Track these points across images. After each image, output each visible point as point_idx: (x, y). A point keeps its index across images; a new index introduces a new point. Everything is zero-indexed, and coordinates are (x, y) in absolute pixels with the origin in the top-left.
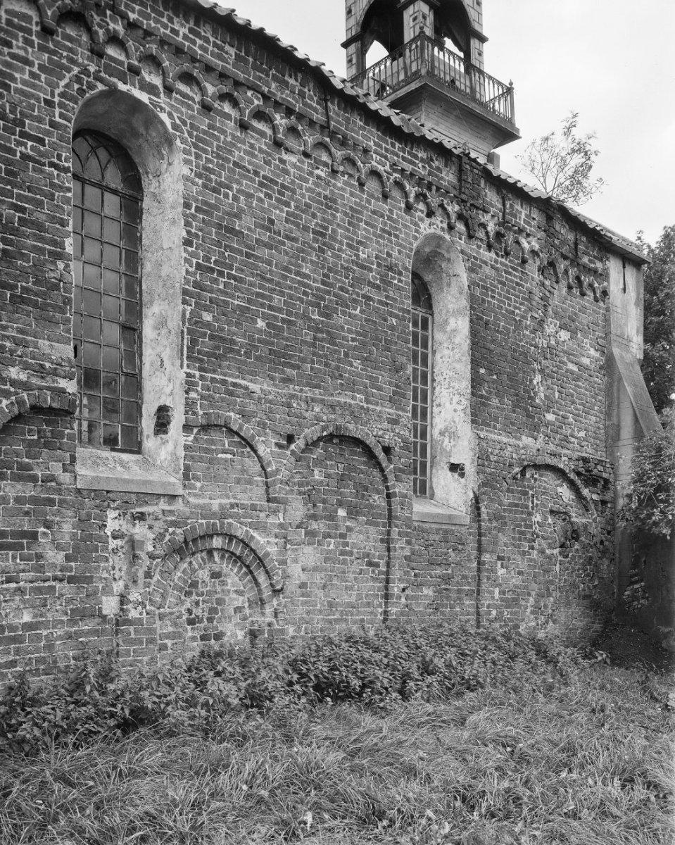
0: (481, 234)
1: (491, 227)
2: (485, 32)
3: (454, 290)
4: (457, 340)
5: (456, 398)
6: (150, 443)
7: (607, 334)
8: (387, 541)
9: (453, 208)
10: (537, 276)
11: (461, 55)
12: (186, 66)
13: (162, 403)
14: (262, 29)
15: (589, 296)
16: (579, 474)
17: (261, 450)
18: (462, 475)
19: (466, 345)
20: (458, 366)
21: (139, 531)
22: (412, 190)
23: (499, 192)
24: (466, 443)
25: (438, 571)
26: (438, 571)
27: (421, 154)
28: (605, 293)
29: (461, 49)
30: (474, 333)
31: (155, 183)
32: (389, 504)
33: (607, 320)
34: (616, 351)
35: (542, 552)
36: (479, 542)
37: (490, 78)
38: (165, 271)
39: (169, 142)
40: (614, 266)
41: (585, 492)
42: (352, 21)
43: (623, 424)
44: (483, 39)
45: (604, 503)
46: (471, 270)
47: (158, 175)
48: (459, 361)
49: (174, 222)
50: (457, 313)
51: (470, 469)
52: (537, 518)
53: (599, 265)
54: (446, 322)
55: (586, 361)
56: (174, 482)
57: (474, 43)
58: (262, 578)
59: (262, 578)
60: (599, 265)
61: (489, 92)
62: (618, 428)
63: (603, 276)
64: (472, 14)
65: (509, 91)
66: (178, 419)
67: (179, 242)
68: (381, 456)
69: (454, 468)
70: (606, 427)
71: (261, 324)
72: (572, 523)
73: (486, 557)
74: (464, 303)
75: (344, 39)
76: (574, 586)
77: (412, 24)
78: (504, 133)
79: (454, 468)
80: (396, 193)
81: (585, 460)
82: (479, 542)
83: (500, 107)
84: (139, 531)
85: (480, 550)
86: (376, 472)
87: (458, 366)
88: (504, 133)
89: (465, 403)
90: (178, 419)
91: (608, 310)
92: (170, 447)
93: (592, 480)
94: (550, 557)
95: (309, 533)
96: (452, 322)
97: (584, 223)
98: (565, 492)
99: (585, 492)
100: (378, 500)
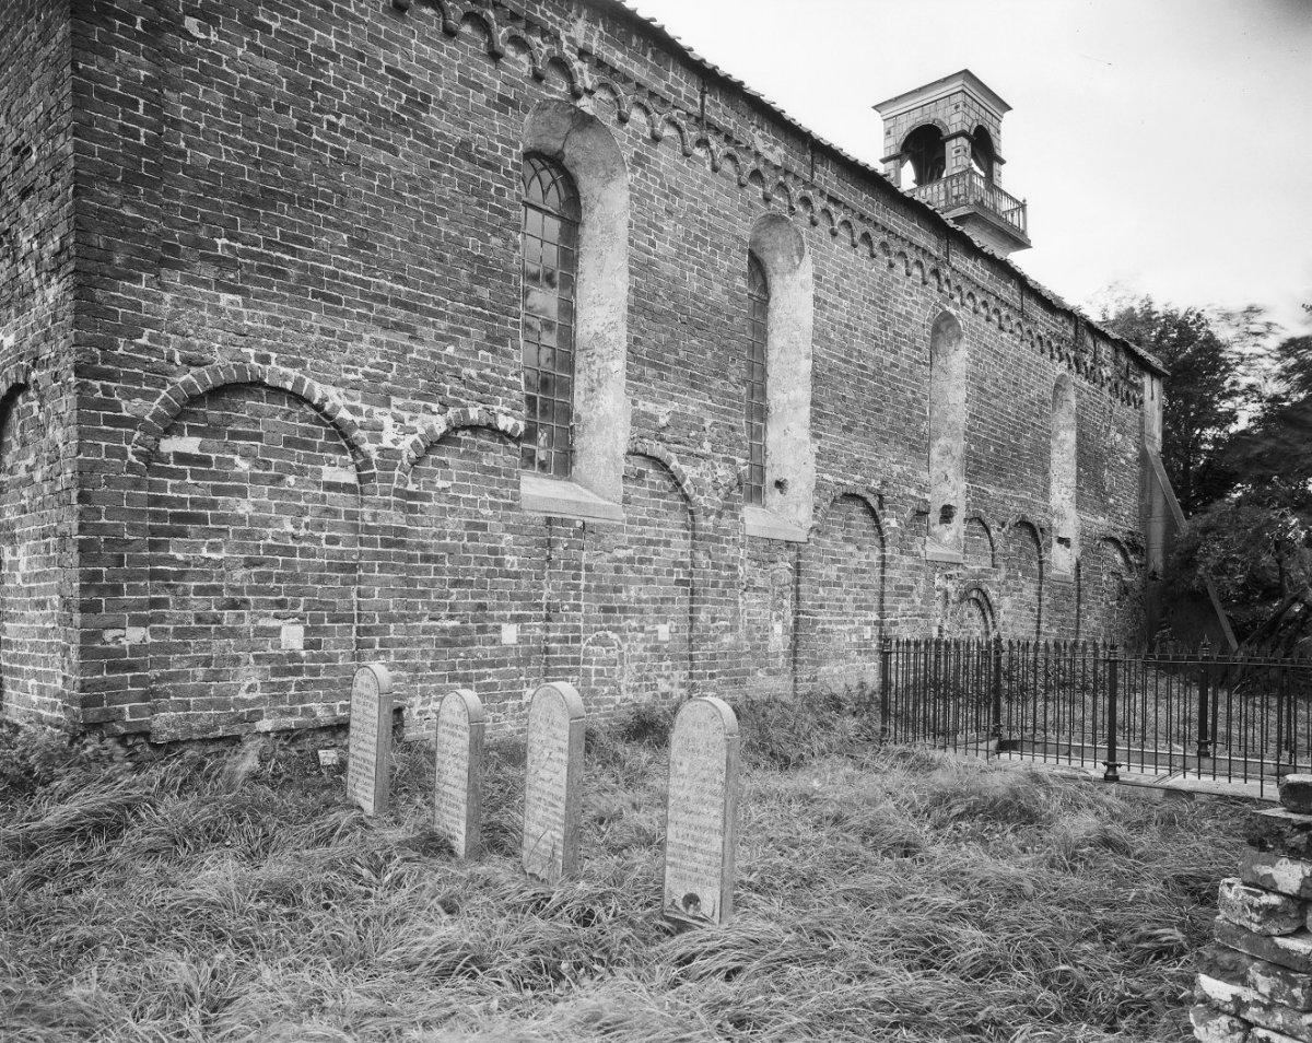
0: (1083, 370)
1: (1089, 364)
2: (1003, 155)
3: (1065, 410)
4: (1066, 447)
5: (1064, 490)
6: (937, 529)
7: (1142, 433)
8: (1039, 594)
9: (1072, 354)
10: (1107, 395)
11: (983, 174)
12: (731, 149)
13: (946, 503)
14: (741, 83)
15: (931, 285)
16: (1128, 544)
17: (993, 533)
18: (1068, 546)
19: (1073, 451)
20: (1066, 466)
21: (950, 586)
22: (819, 204)
23: (1092, 337)
24: (1071, 523)
25: (1060, 616)
26: (1060, 616)
27: (1060, 319)
28: (1141, 402)
29: (982, 169)
30: (1078, 443)
31: (942, 360)
32: (1041, 568)
33: (1142, 423)
34: (1148, 447)
35: (1107, 603)
36: (1079, 596)
37: (1006, 194)
38: (951, 418)
39: (960, 336)
40: (1147, 379)
41: (1131, 557)
42: (891, 142)
43: (1155, 505)
44: (1002, 162)
45: (1141, 566)
46: (1078, 397)
47: (945, 355)
48: (1067, 462)
49: (958, 387)
50: (1068, 427)
51: (1074, 542)
52: (1105, 578)
53: (1139, 381)
54: (1057, 434)
55: (1129, 455)
56: (957, 555)
57: (996, 166)
58: (989, 618)
59: (989, 618)
60: (1139, 381)
61: (1005, 205)
62: (1150, 508)
63: (1140, 388)
64: (995, 141)
65: (1022, 206)
66: (960, 514)
67: (962, 400)
68: (1040, 535)
69: (1061, 540)
70: (1140, 507)
71: (992, 449)
72: (1123, 582)
73: (1082, 607)
74: (1072, 420)
75: (883, 157)
76: (1125, 629)
77: (954, 155)
78: (1019, 241)
79: (1061, 540)
80: (843, 232)
81: (1130, 532)
82: (1079, 596)
83: (1015, 220)
84: (950, 586)
85: (1079, 601)
86: (1035, 546)
87: (1066, 466)
88: (1019, 241)
89: (1072, 493)
90: (960, 514)
91: (1142, 414)
92: (953, 532)
93: (1135, 548)
94: (1111, 607)
95: (1008, 589)
96: (1062, 434)
97: (768, 106)
98: (1118, 557)
99: (1131, 557)
100: (1035, 565)
